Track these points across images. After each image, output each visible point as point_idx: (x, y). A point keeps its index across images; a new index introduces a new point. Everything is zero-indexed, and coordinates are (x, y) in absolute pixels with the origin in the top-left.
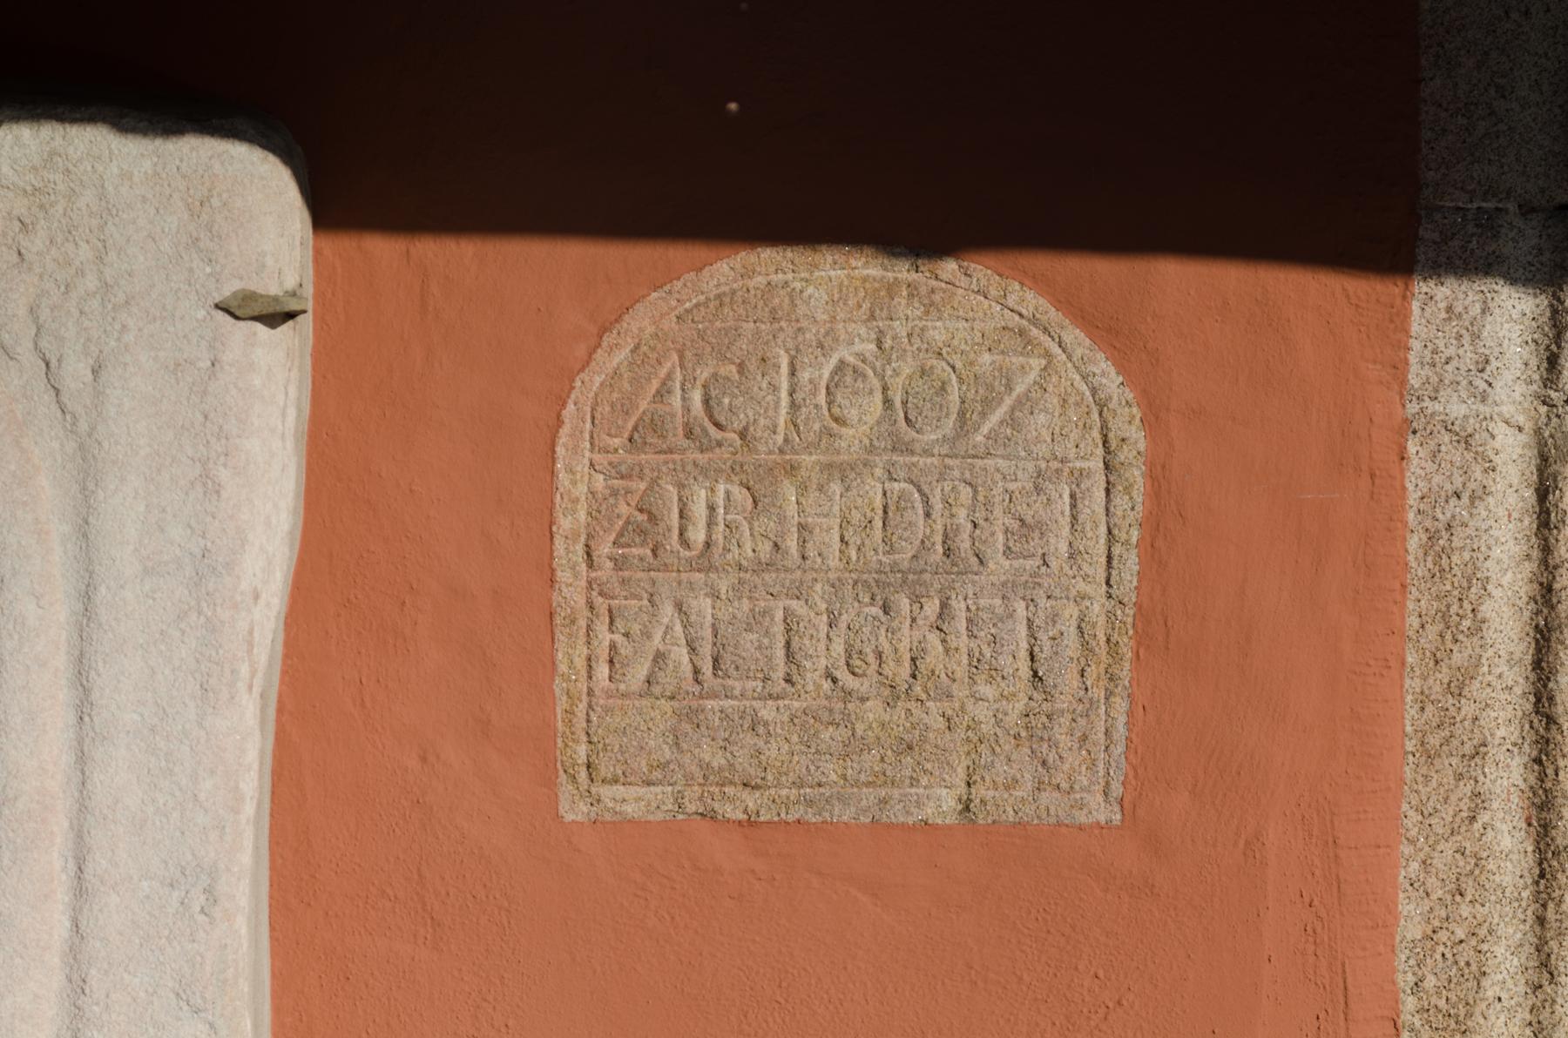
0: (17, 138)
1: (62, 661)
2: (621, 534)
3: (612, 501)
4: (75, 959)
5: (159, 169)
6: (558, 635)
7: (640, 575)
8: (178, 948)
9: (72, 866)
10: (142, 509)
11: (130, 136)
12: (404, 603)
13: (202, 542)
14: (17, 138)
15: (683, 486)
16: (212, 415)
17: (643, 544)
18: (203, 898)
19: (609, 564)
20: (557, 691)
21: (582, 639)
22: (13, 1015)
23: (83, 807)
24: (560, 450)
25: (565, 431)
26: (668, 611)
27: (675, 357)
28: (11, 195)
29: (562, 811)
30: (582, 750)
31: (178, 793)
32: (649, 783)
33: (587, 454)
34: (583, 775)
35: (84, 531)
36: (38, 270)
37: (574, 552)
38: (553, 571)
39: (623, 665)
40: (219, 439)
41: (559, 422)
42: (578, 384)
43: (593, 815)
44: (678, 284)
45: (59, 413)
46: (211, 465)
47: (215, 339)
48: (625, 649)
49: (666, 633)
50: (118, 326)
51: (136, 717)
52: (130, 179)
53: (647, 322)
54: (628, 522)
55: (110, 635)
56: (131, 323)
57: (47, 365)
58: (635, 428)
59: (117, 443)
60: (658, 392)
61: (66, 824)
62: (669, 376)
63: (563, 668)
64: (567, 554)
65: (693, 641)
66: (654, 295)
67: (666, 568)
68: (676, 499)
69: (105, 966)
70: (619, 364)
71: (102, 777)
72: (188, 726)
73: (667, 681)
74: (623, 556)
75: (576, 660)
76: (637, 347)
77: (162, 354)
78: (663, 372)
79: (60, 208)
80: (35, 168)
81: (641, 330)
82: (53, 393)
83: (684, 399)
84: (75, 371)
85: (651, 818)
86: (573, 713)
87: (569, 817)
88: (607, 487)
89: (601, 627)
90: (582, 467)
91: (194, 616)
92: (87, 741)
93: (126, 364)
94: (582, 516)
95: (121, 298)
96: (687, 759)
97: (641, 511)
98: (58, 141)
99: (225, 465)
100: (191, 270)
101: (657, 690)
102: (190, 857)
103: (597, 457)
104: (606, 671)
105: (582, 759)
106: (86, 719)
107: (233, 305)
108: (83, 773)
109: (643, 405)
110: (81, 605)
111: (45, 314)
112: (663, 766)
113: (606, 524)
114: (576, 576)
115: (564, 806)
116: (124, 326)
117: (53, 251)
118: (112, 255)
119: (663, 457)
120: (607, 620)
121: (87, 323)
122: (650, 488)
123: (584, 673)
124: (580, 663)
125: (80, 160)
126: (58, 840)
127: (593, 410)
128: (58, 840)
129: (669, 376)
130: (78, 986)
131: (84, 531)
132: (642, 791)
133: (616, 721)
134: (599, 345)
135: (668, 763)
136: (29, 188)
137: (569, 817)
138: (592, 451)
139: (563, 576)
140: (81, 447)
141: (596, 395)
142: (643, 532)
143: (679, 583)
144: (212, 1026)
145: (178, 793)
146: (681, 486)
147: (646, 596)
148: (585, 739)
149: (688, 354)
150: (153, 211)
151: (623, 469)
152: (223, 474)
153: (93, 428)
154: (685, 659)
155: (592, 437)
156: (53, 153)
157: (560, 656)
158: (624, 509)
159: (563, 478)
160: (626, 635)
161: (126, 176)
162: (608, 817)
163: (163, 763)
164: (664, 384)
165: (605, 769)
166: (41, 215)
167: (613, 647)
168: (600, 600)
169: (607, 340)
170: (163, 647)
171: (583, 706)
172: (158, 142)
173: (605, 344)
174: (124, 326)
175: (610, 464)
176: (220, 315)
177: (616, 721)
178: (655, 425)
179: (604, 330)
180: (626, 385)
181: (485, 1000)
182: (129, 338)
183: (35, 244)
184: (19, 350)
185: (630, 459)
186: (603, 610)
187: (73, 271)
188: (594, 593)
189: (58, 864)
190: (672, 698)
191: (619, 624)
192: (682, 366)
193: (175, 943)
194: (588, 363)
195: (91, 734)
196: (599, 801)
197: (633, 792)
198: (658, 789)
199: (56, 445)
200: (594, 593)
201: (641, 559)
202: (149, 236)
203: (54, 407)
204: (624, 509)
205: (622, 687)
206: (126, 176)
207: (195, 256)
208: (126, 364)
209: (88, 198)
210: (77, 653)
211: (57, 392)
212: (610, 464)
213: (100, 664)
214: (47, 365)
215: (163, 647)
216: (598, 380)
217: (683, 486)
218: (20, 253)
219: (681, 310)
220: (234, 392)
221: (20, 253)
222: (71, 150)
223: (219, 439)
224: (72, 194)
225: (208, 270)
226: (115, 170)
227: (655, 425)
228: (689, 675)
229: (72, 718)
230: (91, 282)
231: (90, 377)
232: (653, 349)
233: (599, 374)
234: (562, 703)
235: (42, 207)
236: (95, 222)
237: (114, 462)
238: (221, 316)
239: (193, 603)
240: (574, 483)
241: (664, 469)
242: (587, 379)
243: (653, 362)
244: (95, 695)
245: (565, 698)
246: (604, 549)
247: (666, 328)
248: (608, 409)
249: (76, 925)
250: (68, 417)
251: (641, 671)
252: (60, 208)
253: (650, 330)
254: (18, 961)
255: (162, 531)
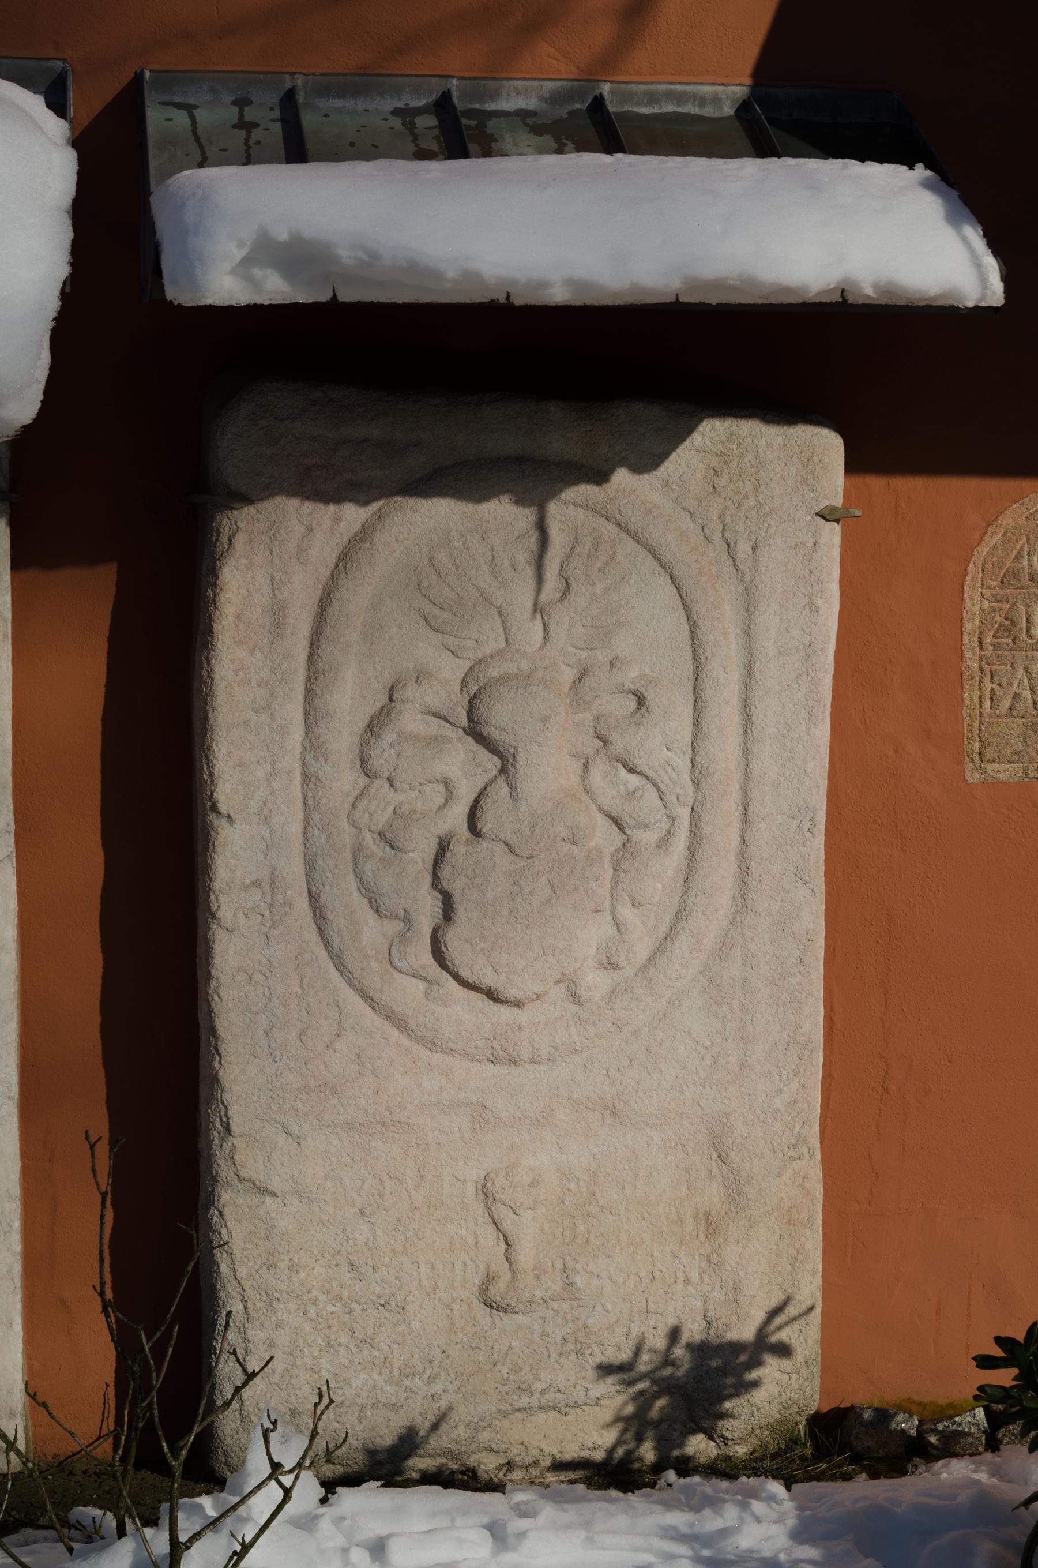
0: (713, 426)
1: (735, 701)
2: (997, 632)
3: (993, 614)
4: (743, 857)
5: (786, 442)
6: (965, 685)
7: (1006, 653)
8: (796, 851)
9: (741, 809)
10: (778, 621)
11: (771, 425)
12: (886, 669)
13: (809, 638)
14: (713, 426)
15: (1029, 606)
16: (814, 571)
17: (1008, 637)
18: (809, 824)
19: (991, 648)
20: (964, 714)
21: (977, 688)
22: (712, 887)
23: (747, 777)
24: (966, 588)
25: (969, 578)
26: (1020, 671)
27: (1025, 538)
28: (709, 456)
29: (967, 777)
30: (977, 745)
31: (796, 769)
32: (1011, 762)
33: (980, 590)
34: (977, 757)
35: (748, 633)
36: (723, 496)
37: (973, 641)
38: (962, 651)
39: (998, 701)
40: (818, 584)
41: (966, 573)
42: (976, 553)
43: (982, 779)
44: (1027, 500)
45: (735, 570)
46: (814, 597)
47: (816, 532)
48: (999, 692)
49: (1019, 683)
50: (766, 525)
51: (775, 730)
52: (772, 447)
53: (1011, 520)
54: (1000, 625)
55: (762, 687)
56: (772, 523)
57: (729, 546)
58: (1004, 576)
59: (765, 586)
60: (1016, 557)
61: (738, 786)
62: (1022, 549)
63: (967, 702)
64: (970, 642)
65: (1033, 687)
66: (1014, 506)
67: (1020, 649)
68: (1024, 613)
69: (759, 860)
70: (996, 543)
71: (757, 762)
72: (801, 734)
73: (1020, 707)
74: (998, 643)
75: (974, 698)
76: (1005, 534)
77: (788, 539)
78: (1018, 546)
79: (735, 463)
80: (722, 442)
81: (1008, 524)
82: (731, 560)
83: (1029, 560)
84: (743, 549)
85: (1012, 780)
86: (973, 726)
87: (970, 780)
88: (990, 607)
89: (987, 680)
90: (977, 597)
91: (805, 677)
92: (749, 742)
93: (770, 545)
94: (977, 622)
95: (767, 510)
96: (1030, 749)
97: (1007, 619)
98: (734, 427)
99: (821, 597)
100: (803, 495)
101: (1015, 713)
102: (802, 803)
103: (985, 591)
104: (989, 703)
105: (977, 750)
106: (749, 731)
107: (826, 513)
108: (747, 759)
109: (1008, 564)
110: (746, 671)
111: (727, 519)
112: (1018, 753)
113: (989, 626)
114: (974, 654)
115: (968, 775)
116: (769, 525)
117: (732, 485)
118: (763, 487)
119: (1018, 591)
120: (989, 676)
121: (750, 524)
122: (1012, 607)
123: (978, 705)
124: (976, 699)
125: (746, 437)
126: (734, 795)
127: (983, 566)
128: (734, 795)
129: (1022, 549)
130: (744, 871)
131: (748, 633)
132: (1007, 766)
133: (995, 729)
134: (986, 533)
135: (1021, 751)
136: (719, 452)
137: (970, 780)
138: (982, 588)
139: (968, 654)
140: (746, 589)
141: (985, 559)
142: (1009, 631)
143: (1027, 657)
144: (813, 891)
145: (796, 769)
146: (1027, 606)
147: (1009, 664)
148: (978, 739)
149: (1032, 537)
150: (783, 464)
151: (998, 597)
152: (820, 602)
153: (753, 579)
154: (1029, 697)
155: (982, 581)
156: (732, 434)
157: (966, 695)
158: (998, 619)
159: (968, 603)
160: (999, 685)
161: (769, 445)
162: (990, 780)
163: (789, 754)
164: (1019, 552)
165: (989, 754)
166: (725, 466)
167: (993, 691)
168: (986, 666)
169: (990, 530)
170: (789, 693)
171: (977, 722)
172: (785, 428)
173: (989, 532)
174: (769, 525)
175: (992, 595)
176: (818, 519)
177: (995, 729)
178: (1015, 574)
179: (989, 525)
180: (1000, 553)
181: (928, 877)
182: (772, 531)
183: (722, 482)
184: (714, 538)
185: (1002, 592)
186: (988, 672)
187: (742, 496)
188: (983, 663)
189: (734, 807)
190: (1023, 717)
191: (996, 679)
192: (1028, 543)
193: (795, 848)
194: (981, 542)
195: (752, 739)
196: (985, 772)
197: (1003, 767)
198: (1016, 765)
199: (733, 587)
200: (983, 663)
201: (1008, 645)
202: (781, 477)
203: (732, 568)
204: (998, 619)
205: (998, 712)
206: (769, 445)
207: (805, 488)
208: (770, 545)
209: (749, 457)
210: (744, 697)
211: (734, 560)
212: (992, 595)
213: (757, 702)
214: (729, 546)
215: (789, 693)
216: (986, 550)
217: (1029, 606)
218: (714, 487)
219: (1028, 513)
220: (825, 559)
221: (714, 487)
222: (741, 432)
223: (818, 584)
224: (741, 456)
225: (812, 495)
226: (764, 443)
227: (1015, 574)
228: (1031, 706)
229: (741, 731)
230: (751, 502)
231: (750, 552)
232: (1013, 534)
233: (986, 547)
234: (967, 720)
235: (725, 462)
236: (753, 470)
237: (764, 596)
238: (819, 519)
239: (804, 670)
240: (973, 605)
241: (1019, 597)
242: (980, 550)
243: (1014, 541)
244: (754, 719)
245: (968, 718)
246: (988, 639)
247: (1020, 522)
248: (990, 566)
249: (743, 839)
250: (740, 573)
251: (1007, 703)
252: (735, 463)
253: (1012, 524)
254: (714, 858)
255: (789, 632)
